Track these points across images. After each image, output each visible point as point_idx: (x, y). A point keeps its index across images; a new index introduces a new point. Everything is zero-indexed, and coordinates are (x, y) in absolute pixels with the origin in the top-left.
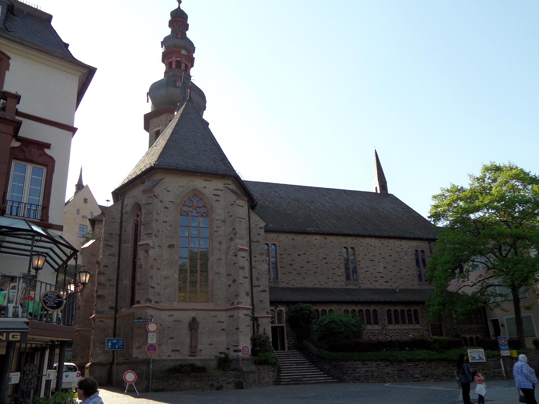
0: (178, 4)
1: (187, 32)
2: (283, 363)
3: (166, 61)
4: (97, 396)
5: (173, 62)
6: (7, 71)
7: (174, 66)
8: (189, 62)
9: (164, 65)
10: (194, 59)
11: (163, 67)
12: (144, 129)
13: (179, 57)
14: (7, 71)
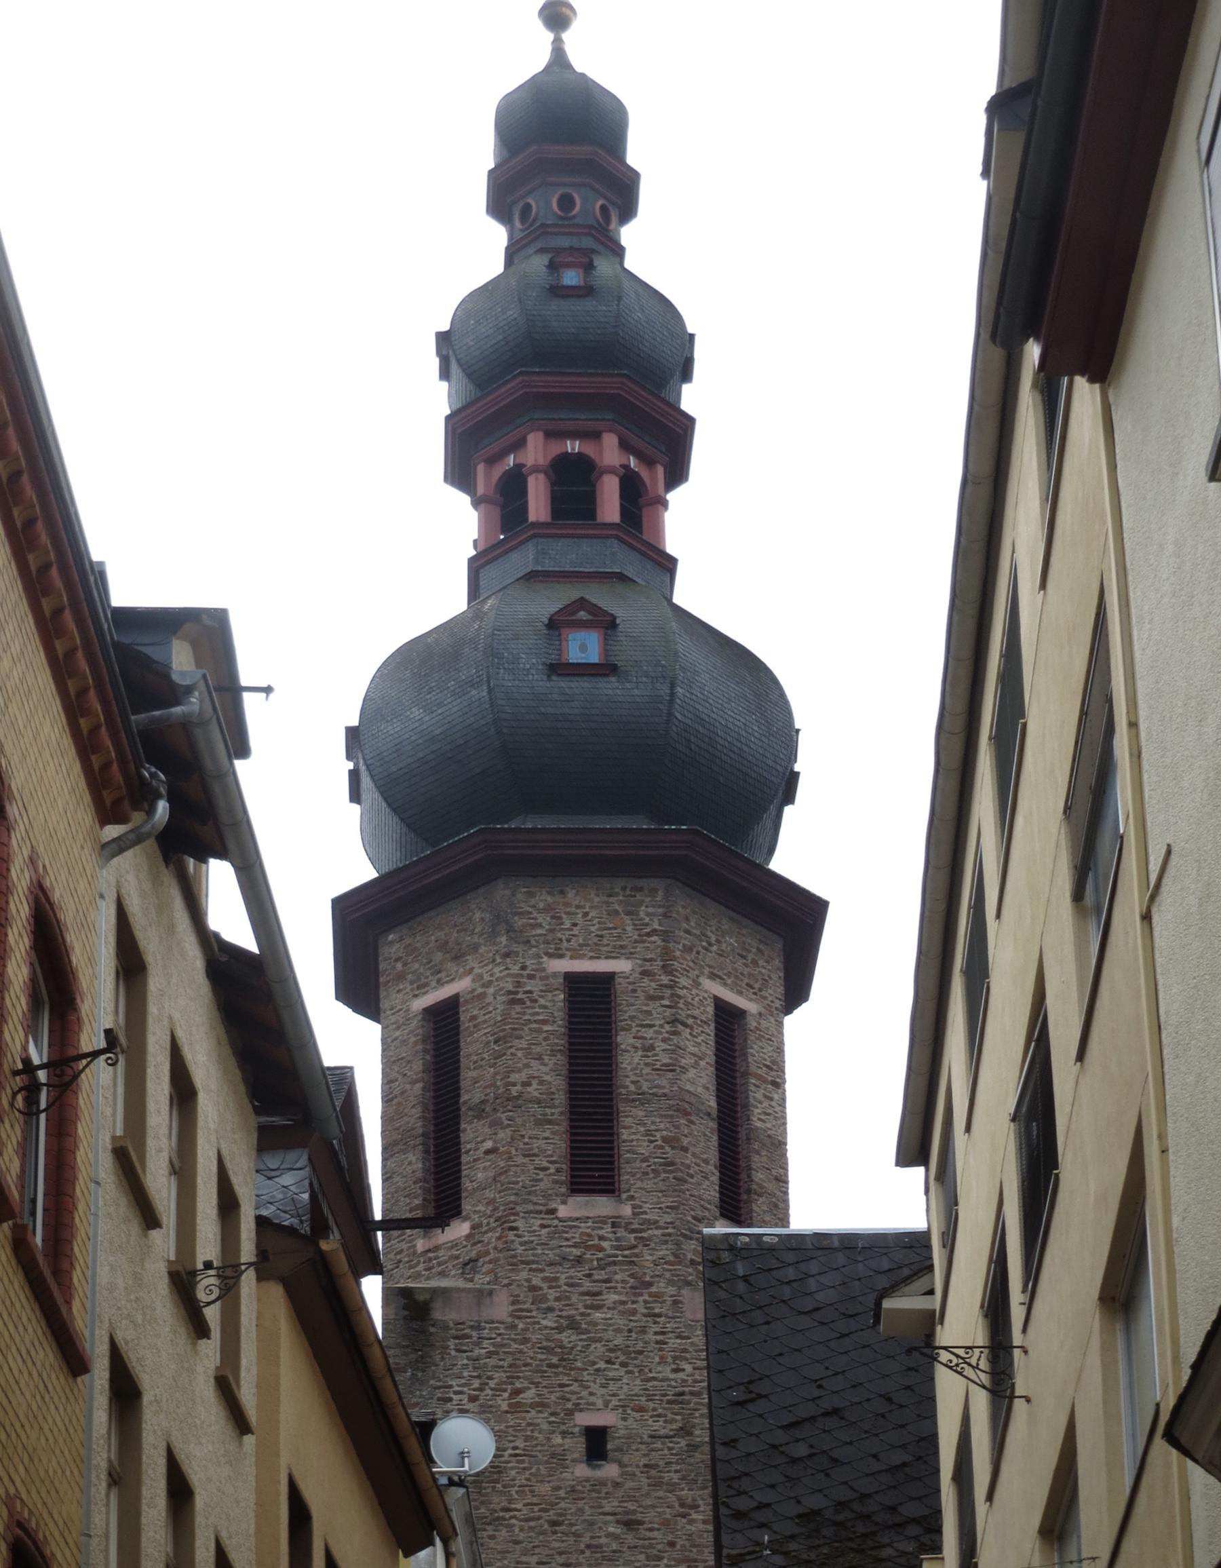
0: (550, 36)
1: (628, 234)
2: (588, 1086)
3: (484, 479)
4: (483, 506)
5: (531, 481)
6: (239, 764)
7: (538, 506)
8: (649, 462)
9: (464, 500)
10: (686, 424)
11: (497, 236)
12: (337, 998)
13: (573, 435)
14: (239, 764)
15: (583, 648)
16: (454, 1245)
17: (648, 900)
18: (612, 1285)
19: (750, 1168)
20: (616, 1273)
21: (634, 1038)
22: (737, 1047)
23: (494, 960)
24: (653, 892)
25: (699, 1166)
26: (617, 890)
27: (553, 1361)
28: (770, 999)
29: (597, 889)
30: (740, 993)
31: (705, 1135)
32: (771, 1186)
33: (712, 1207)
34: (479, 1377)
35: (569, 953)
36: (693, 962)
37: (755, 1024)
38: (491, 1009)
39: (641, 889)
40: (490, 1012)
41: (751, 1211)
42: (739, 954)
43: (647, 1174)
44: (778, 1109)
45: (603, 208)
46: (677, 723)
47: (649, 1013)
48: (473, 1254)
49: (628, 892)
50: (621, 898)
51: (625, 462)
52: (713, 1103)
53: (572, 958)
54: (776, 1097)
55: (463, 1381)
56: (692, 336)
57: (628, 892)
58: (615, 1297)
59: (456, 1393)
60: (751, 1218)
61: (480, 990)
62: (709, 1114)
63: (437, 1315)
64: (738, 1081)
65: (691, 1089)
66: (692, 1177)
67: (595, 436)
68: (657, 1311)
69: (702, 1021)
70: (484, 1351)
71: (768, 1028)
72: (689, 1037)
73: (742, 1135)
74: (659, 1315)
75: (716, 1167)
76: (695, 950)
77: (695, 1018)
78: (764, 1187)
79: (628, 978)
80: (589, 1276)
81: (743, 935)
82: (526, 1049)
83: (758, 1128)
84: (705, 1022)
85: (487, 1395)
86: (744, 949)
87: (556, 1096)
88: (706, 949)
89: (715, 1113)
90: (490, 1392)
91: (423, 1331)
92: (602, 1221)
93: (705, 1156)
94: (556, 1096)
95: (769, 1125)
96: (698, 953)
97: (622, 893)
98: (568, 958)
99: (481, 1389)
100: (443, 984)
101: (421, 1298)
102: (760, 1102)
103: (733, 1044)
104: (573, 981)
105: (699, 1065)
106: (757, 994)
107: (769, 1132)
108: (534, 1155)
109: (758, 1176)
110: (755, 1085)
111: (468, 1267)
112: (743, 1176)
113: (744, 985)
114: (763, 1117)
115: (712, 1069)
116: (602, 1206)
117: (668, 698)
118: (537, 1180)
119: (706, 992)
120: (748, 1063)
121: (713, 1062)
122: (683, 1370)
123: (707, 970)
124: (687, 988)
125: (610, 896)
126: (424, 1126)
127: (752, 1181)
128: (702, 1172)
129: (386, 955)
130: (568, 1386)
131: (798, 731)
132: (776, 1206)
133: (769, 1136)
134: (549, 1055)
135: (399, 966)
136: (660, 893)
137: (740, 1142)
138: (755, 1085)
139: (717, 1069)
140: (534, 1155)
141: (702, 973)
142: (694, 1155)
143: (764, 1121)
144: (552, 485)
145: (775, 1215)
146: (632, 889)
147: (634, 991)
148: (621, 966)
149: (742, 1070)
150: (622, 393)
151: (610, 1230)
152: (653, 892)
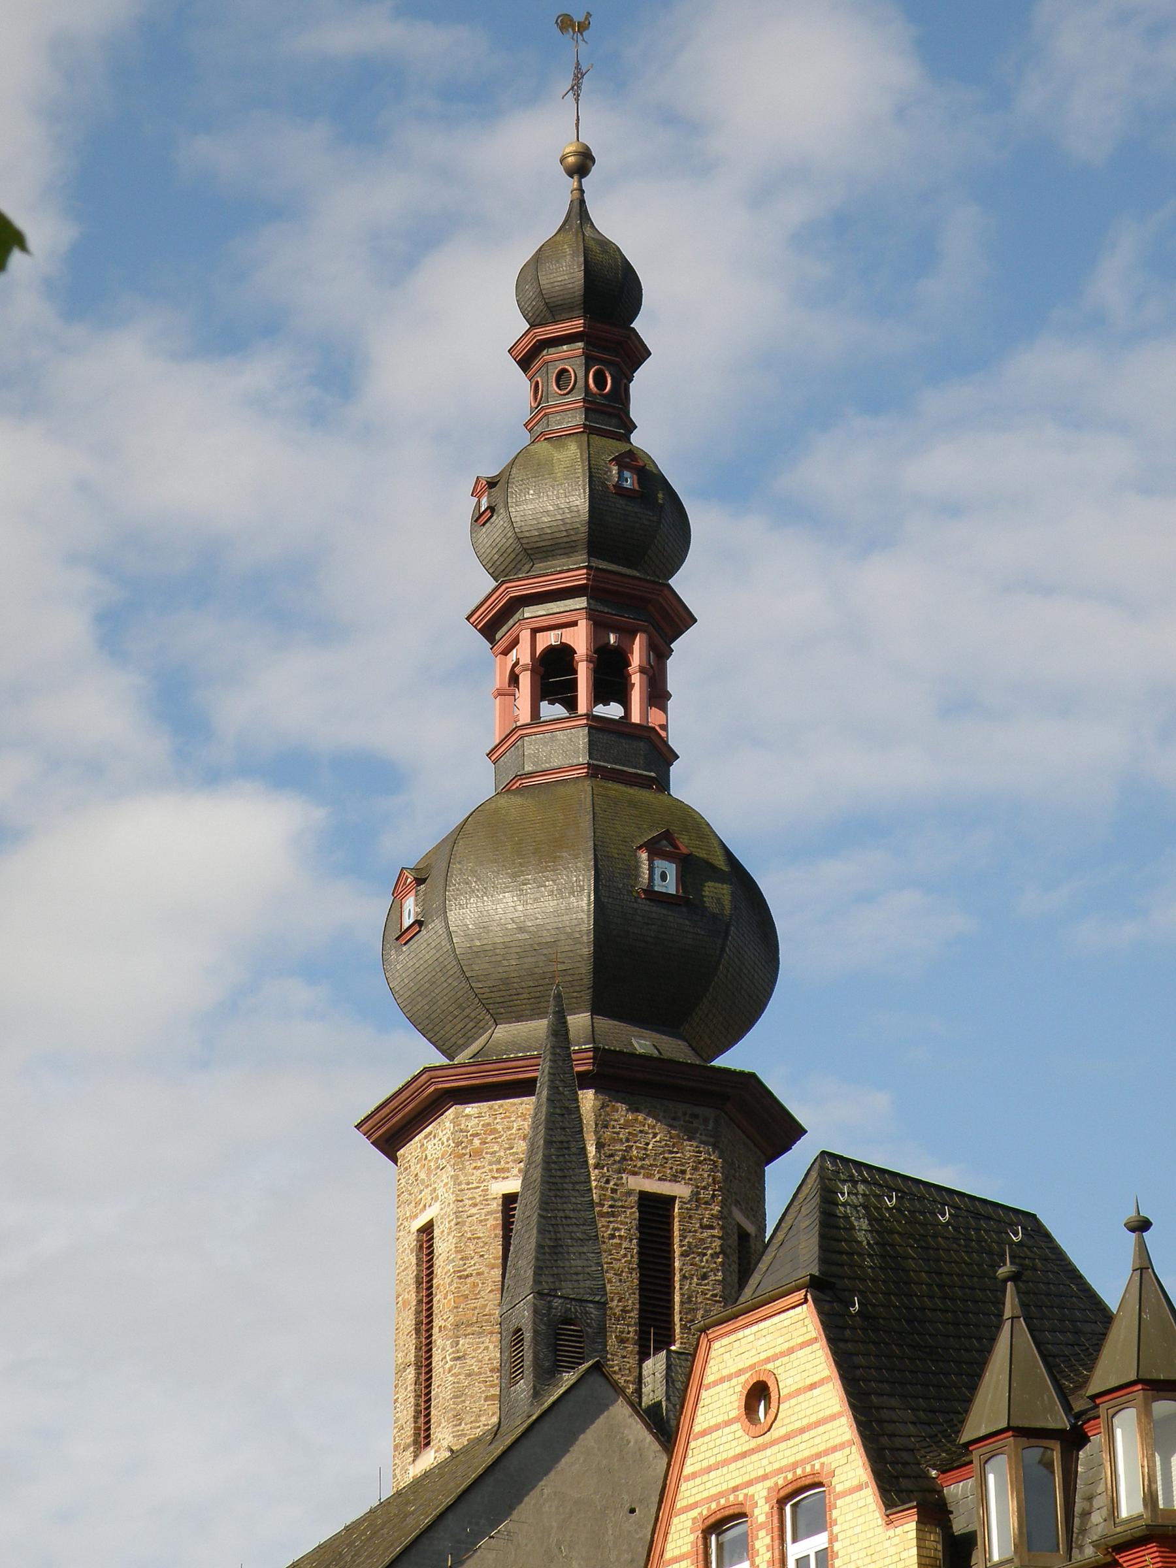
14: (547, 702)
39: (696, 1116)
57: (687, 1118)
98: (641, 1176)
126: (577, 869)
135: (477, 1142)
148: (680, 1190)
150: (512, 595)
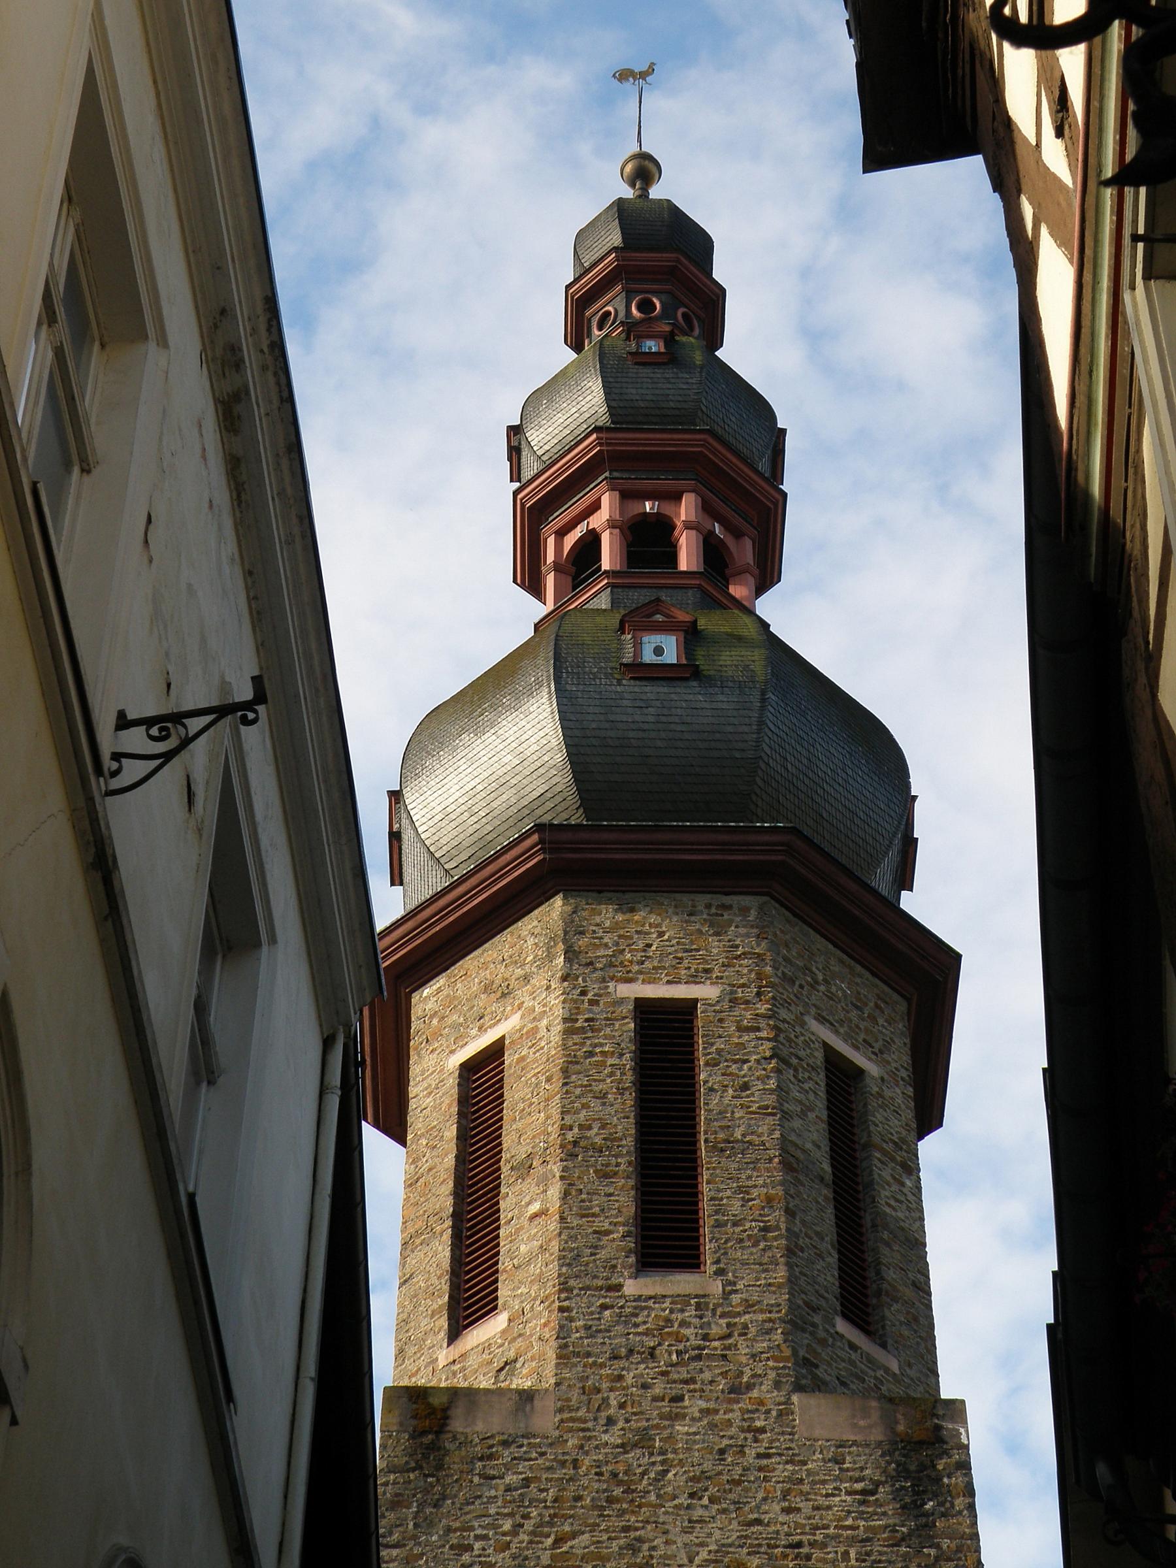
15: (658, 651)
16: (486, 1347)
17: (738, 919)
18: (697, 1386)
19: (878, 1263)
20: (701, 1371)
21: (723, 1075)
22: (854, 1114)
23: (548, 987)
24: (744, 911)
25: (811, 1238)
26: (700, 908)
27: (614, 1493)
28: (894, 1065)
29: (676, 907)
30: (856, 1048)
31: (817, 1202)
32: (908, 1293)
33: (830, 1296)
34: (511, 1515)
35: (641, 977)
36: (795, 995)
37: (875, 1089)
38: (543, 1044)
39: (730, 907)
40: (542, 1048)
41: (883, 1318)
42: (852, 1003)
43: (741, 1241)
44: (911, 1197)
45: (684, 315)
46: (770, 734)
47: (742, 1046)
48: (512, 1354)
49: (713, 910)
50: (705, 916)
51: (709, 527)
52: (827, 1167)
53: (644, 982)
54: (908, 1183)
55: (487, 1521)
56: (783, 432)
58: (702, 1404)
59: (477, 1538)
60: (883, 1327)
61: (530, 1026)
62: (822, 1179)
63: (457, 1424)
64: (858, 1155)
65: (798, 1142)
66: (802, 1250)
67: (677, 497)
68: (758, 1424)
69: (808, 1065)
70: (521, 1477)
71: (892, 1098)
72: (792, 1079)
73: (867, 1220)
74: (762, 1430)
75: (833, 1246)
76: (797, 983)
77: (800, 1059)
78: (898, 1291)
79: (714, 1006)
80: (664, 1374)
81: (857, 984)
82: (586, 1086)
83: (886, 1214)
84: (813, 1068)
85: (521, 1542)
86: (860, 1000)
87: (624, 1142)
88: (812, 987)
89: (829, 1177)
90: (526, 1538)
91: (434, 1447)
92: (682, 1300)
93: (818, 1229)
94: (624, 1142)
95: (900, 1214)
96: (801, 987)
97: (705, 911)
99: (514, 1532)
100: (486, 1030)
101: (436, 1401)
102: (888, 1184)
103: (852, 1110)
104: (644, 1008)
105: (806, 1116)
106: (878, 1055)
107: (902, 1224)
108: (594, 1215)
109: (891, 1275)
110: (879, 1160)
111: (504, 1372)
112: (871, 1274)
113: (860, 1040)
114: (892, 1203)
115: (825, 1126)
116: (682, 1283)
117: (759, 704)
118: (596, 1247)
119: (813, 1034)
120: (869, 1133)
121: (825, 1117)
122: (798, 1510)
123: (813, 1011)
124: (788, 1023)
125: (690, 914)
127: (882, 1279)
128: (815, 1247)
129: (420, 1013)
130: (637, 1529)
131: (915, 798)
132: (916, 1319)
133: (903, 1229)
134: (615, 1094)
136: (753, 913)
137: (864, 1230)
138: (879, 1160)
139: (830, 1124)
140: (594, 1215)
141: (808, 1013)
142: (803, 1222)
143: (894, 1209)
144: (628, 546)
145: (916, 1332)
146: (718, 907)
147: (721, 1020)
148: (706, 992)
149: (862, 1141)
151: (694, 1313)
152: (744, 911)
